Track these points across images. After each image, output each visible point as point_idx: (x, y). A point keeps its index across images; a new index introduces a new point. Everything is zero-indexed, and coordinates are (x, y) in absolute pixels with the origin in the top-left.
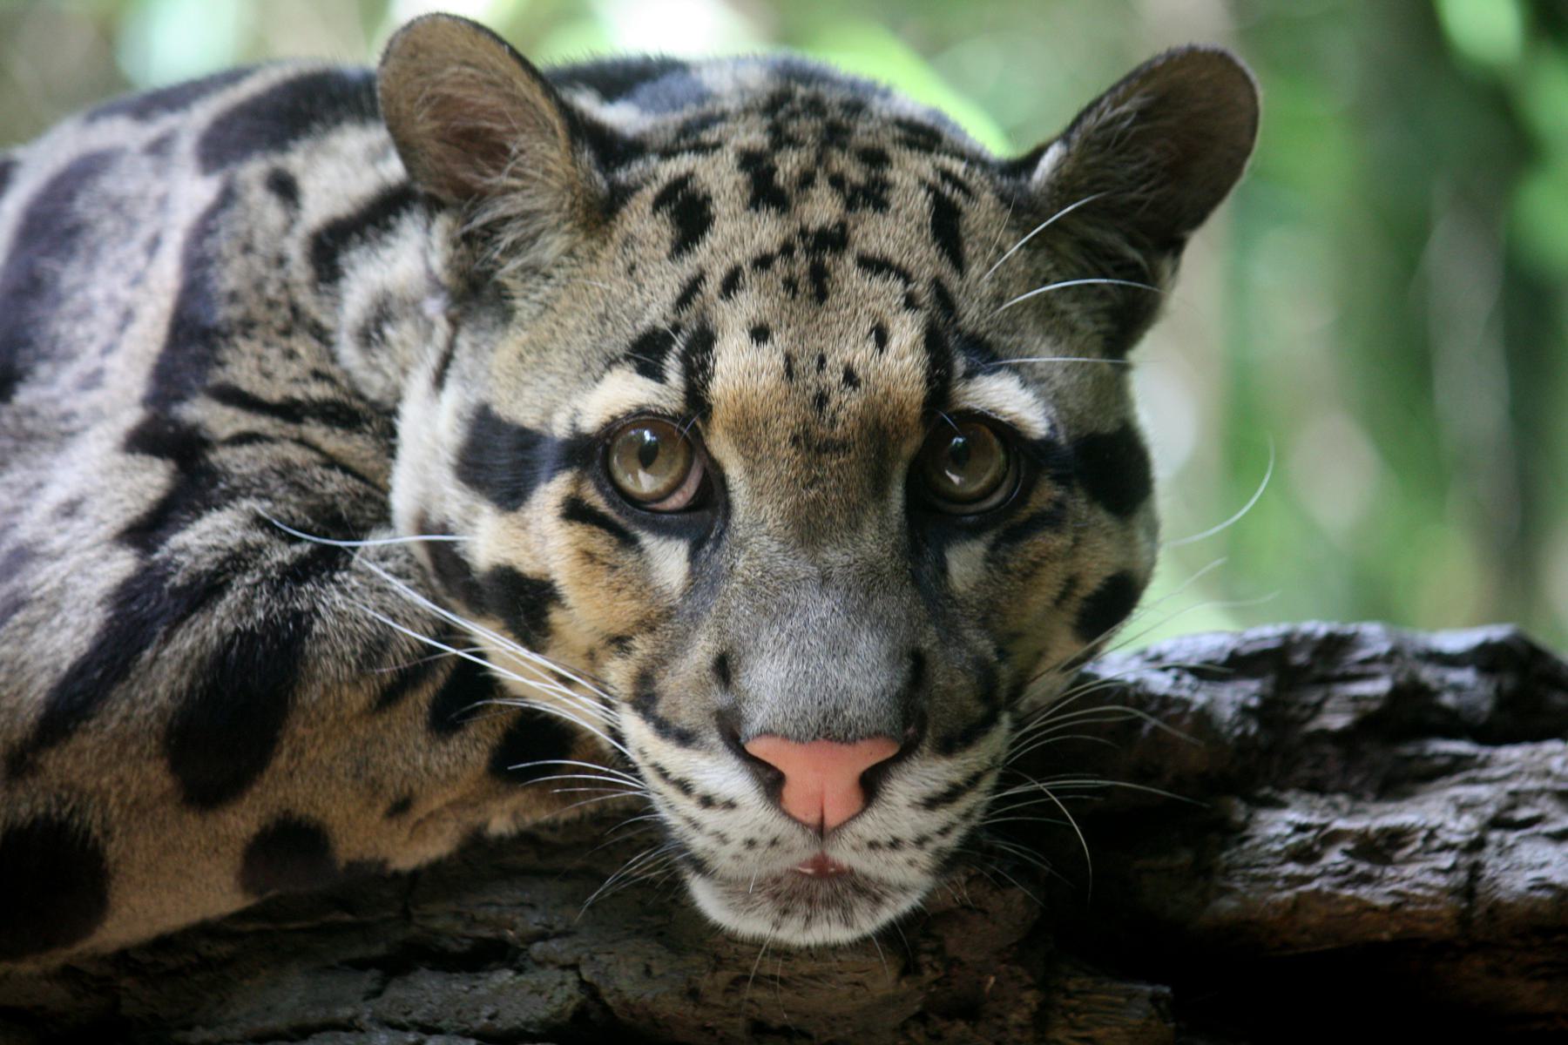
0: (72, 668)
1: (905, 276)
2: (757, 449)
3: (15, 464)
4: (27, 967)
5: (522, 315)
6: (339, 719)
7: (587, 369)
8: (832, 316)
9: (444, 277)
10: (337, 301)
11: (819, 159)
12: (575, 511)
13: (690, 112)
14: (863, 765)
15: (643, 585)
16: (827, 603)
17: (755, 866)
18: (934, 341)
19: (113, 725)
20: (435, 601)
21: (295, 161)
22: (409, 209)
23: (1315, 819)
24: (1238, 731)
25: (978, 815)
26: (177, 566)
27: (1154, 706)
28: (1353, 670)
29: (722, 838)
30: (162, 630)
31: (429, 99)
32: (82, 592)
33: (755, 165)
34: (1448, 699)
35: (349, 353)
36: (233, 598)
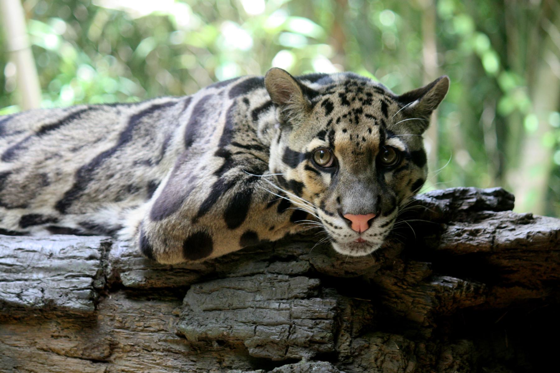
0: (205, 201)
1: (375, 118)
2: (344, 154)
3: (192, 159)
4: (197, 262)
5: (294, 128)
6: (259, 210)
7: (309, 139)
8: (360, 127)
9: (279, 120)
10: (257, 125)
11: (356, 95)
12: (307, 168)
13: (328, 85)
14: (368, 219)
15: (322, 183)
16: (360, 186)
17: (346, 240)
18: (381, 131)
19: (213, 212)
20: (278, 186)
21: (249, 96)
22: (272, 106)
23: (461, 228)
24: (445, 210)
25: (392, 228)
26: (226, 179)
27: (427, 205)
28: (469, 197)
29: (339, 235)
30: (222, 193)
31: (275, 84)
32: (206, 185)
33: (342, 96)
34: (488, 202)
35: (260, 135)
36: (237, 186)
